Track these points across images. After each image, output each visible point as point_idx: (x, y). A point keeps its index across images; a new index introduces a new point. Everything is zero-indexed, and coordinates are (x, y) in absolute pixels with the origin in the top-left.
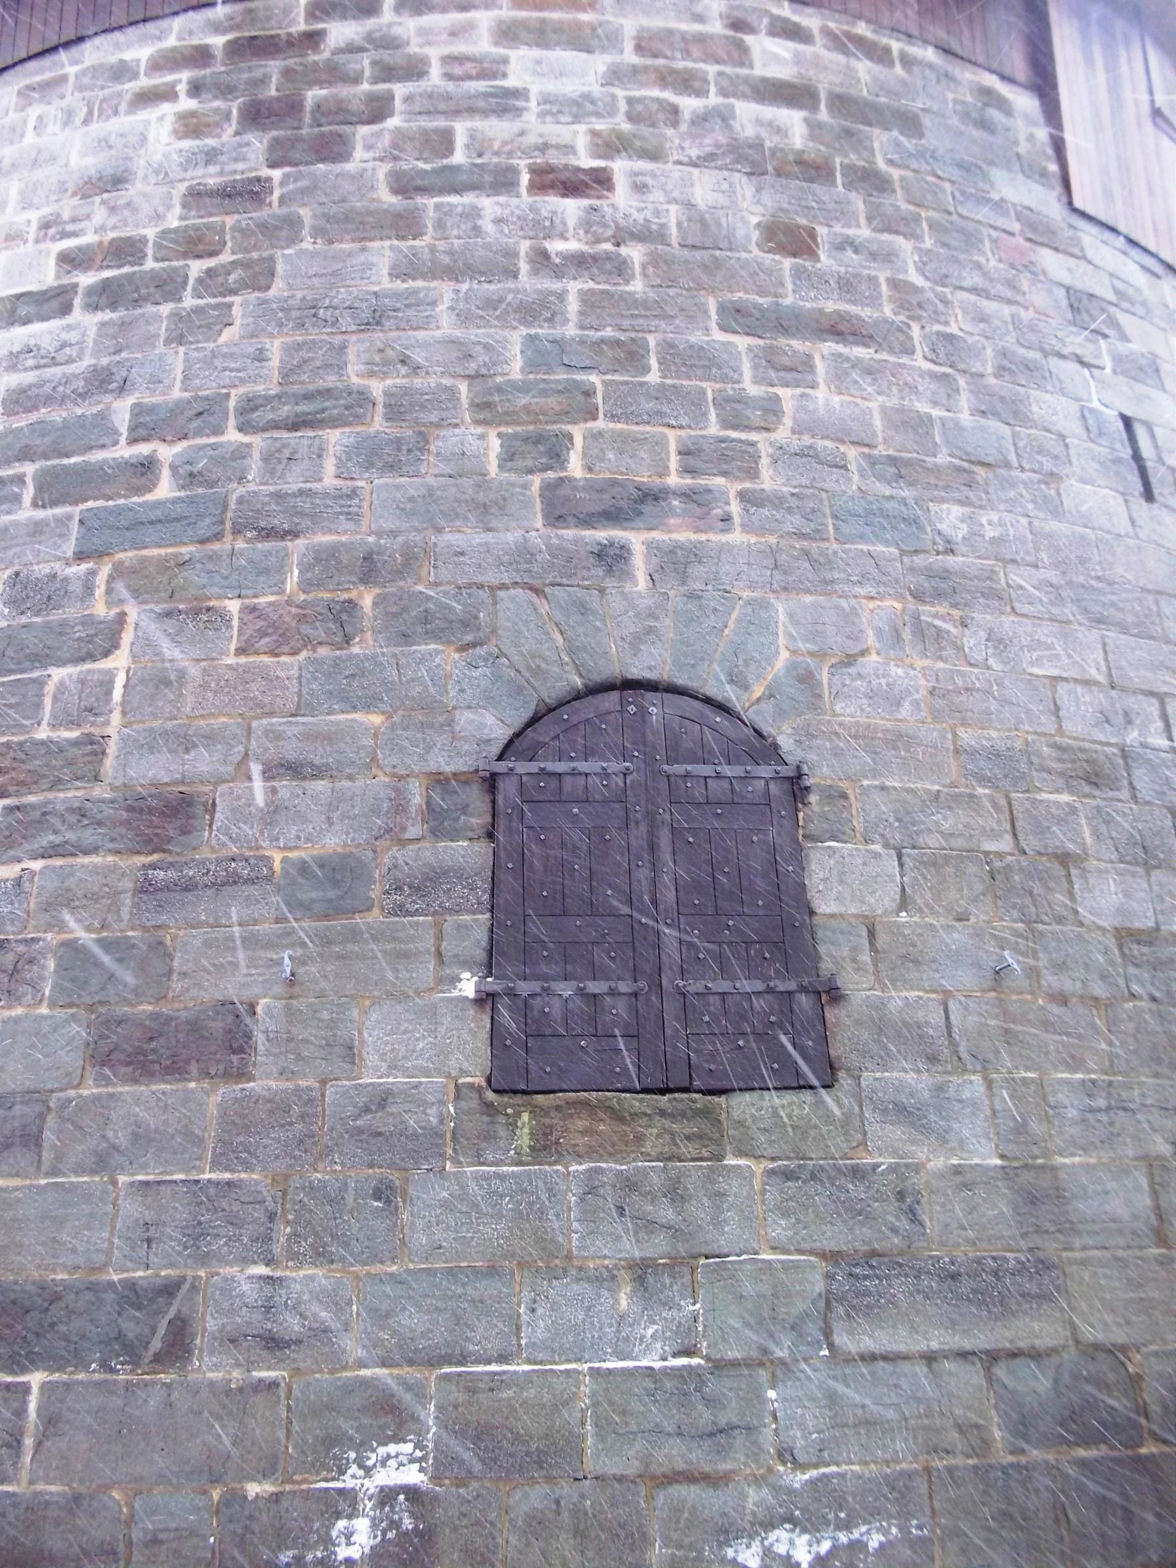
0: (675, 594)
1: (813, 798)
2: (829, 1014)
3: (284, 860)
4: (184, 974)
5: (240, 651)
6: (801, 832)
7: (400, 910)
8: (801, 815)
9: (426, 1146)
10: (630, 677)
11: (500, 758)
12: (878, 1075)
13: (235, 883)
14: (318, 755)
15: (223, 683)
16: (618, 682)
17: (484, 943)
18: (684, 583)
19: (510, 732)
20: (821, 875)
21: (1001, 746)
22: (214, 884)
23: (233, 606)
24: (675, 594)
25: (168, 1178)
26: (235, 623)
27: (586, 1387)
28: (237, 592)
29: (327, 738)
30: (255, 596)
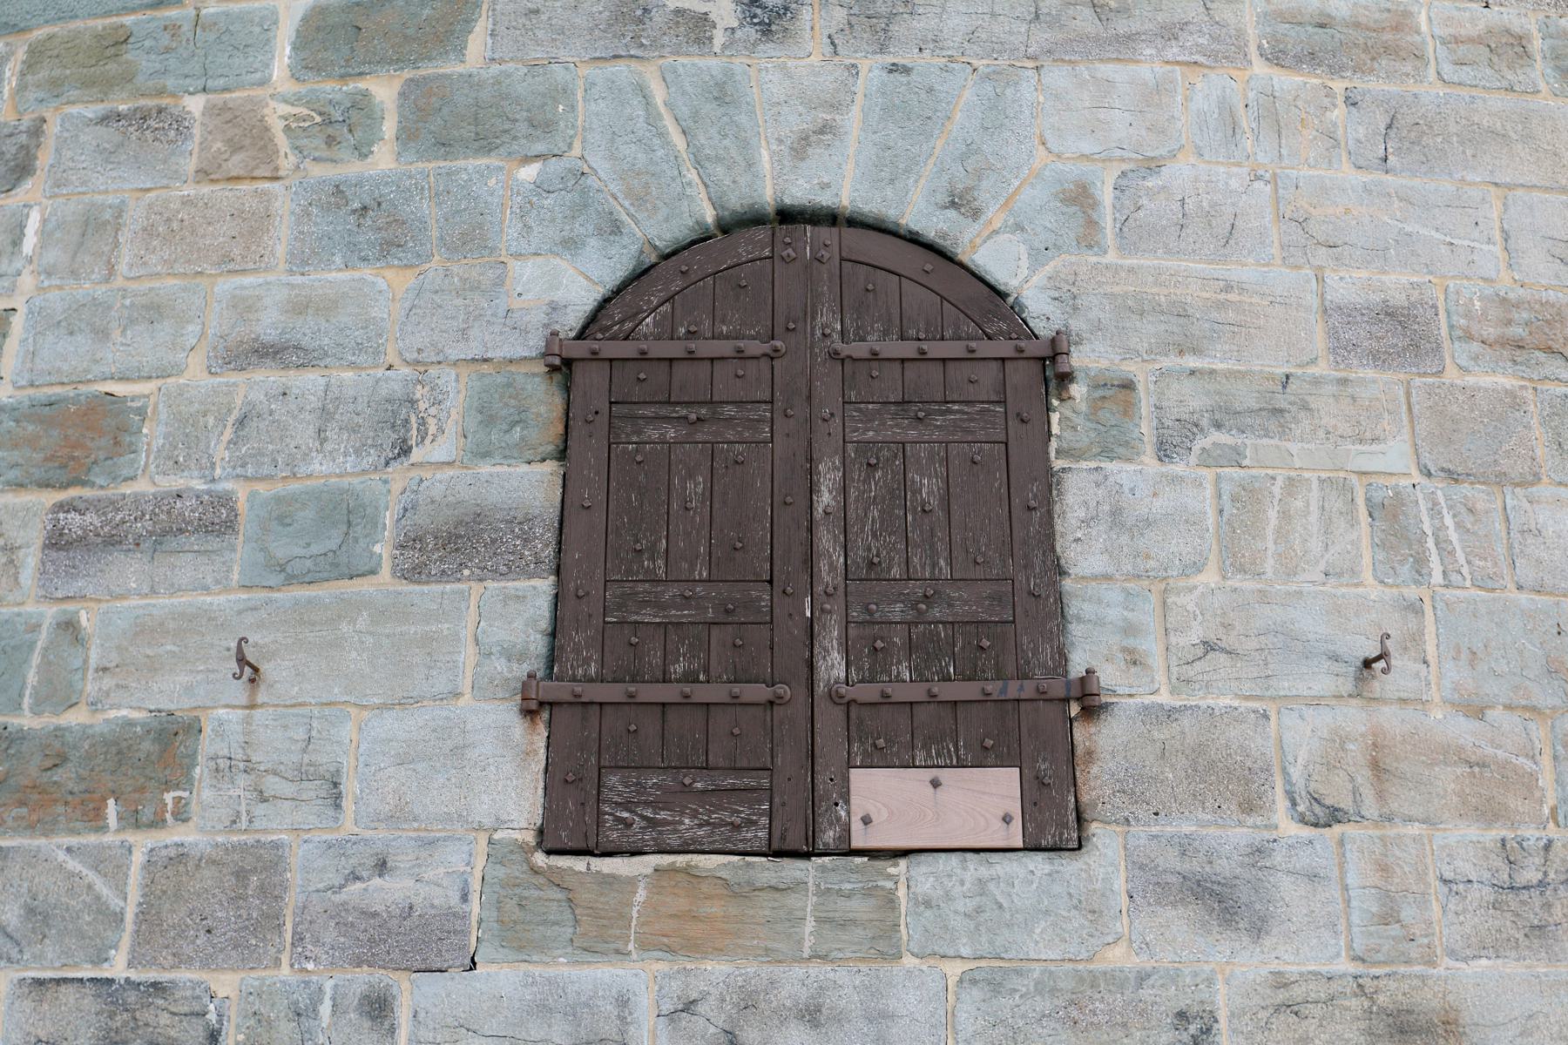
0: (871, 68)
1: (1077, 390)
2: (1080, 732)
3: (253, 495)
4: (105, 669)
5: (203, 174)
6: (1054, 444)
7: (415, 573)
8: (1055, 417)
9: (429, 944)
10: (788, 201)
11: (581, 336)
12: (1155, 830)
13: (181, 531)
14: (306, 330)
15: (175, 225)
16: (770, 210)
17: (545, 624)
18: (882, 49)
19: (598, 293)
20: (1082, 514)
21: (1399, 299)
22: (151, 533)
23: (195, 105)
24: (871, 68)
25: (71, 975)
26: (197, 131)
27: (1260, 545)
28: (200, 83)
29: (328, 306)
30: (226, 90)
